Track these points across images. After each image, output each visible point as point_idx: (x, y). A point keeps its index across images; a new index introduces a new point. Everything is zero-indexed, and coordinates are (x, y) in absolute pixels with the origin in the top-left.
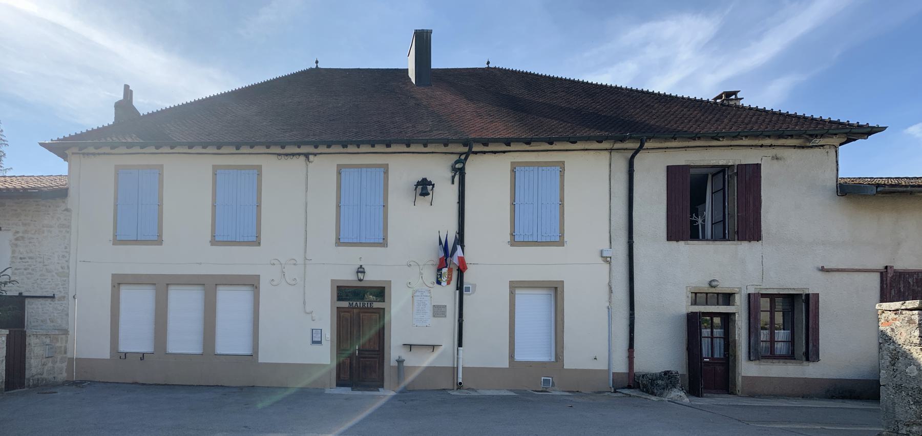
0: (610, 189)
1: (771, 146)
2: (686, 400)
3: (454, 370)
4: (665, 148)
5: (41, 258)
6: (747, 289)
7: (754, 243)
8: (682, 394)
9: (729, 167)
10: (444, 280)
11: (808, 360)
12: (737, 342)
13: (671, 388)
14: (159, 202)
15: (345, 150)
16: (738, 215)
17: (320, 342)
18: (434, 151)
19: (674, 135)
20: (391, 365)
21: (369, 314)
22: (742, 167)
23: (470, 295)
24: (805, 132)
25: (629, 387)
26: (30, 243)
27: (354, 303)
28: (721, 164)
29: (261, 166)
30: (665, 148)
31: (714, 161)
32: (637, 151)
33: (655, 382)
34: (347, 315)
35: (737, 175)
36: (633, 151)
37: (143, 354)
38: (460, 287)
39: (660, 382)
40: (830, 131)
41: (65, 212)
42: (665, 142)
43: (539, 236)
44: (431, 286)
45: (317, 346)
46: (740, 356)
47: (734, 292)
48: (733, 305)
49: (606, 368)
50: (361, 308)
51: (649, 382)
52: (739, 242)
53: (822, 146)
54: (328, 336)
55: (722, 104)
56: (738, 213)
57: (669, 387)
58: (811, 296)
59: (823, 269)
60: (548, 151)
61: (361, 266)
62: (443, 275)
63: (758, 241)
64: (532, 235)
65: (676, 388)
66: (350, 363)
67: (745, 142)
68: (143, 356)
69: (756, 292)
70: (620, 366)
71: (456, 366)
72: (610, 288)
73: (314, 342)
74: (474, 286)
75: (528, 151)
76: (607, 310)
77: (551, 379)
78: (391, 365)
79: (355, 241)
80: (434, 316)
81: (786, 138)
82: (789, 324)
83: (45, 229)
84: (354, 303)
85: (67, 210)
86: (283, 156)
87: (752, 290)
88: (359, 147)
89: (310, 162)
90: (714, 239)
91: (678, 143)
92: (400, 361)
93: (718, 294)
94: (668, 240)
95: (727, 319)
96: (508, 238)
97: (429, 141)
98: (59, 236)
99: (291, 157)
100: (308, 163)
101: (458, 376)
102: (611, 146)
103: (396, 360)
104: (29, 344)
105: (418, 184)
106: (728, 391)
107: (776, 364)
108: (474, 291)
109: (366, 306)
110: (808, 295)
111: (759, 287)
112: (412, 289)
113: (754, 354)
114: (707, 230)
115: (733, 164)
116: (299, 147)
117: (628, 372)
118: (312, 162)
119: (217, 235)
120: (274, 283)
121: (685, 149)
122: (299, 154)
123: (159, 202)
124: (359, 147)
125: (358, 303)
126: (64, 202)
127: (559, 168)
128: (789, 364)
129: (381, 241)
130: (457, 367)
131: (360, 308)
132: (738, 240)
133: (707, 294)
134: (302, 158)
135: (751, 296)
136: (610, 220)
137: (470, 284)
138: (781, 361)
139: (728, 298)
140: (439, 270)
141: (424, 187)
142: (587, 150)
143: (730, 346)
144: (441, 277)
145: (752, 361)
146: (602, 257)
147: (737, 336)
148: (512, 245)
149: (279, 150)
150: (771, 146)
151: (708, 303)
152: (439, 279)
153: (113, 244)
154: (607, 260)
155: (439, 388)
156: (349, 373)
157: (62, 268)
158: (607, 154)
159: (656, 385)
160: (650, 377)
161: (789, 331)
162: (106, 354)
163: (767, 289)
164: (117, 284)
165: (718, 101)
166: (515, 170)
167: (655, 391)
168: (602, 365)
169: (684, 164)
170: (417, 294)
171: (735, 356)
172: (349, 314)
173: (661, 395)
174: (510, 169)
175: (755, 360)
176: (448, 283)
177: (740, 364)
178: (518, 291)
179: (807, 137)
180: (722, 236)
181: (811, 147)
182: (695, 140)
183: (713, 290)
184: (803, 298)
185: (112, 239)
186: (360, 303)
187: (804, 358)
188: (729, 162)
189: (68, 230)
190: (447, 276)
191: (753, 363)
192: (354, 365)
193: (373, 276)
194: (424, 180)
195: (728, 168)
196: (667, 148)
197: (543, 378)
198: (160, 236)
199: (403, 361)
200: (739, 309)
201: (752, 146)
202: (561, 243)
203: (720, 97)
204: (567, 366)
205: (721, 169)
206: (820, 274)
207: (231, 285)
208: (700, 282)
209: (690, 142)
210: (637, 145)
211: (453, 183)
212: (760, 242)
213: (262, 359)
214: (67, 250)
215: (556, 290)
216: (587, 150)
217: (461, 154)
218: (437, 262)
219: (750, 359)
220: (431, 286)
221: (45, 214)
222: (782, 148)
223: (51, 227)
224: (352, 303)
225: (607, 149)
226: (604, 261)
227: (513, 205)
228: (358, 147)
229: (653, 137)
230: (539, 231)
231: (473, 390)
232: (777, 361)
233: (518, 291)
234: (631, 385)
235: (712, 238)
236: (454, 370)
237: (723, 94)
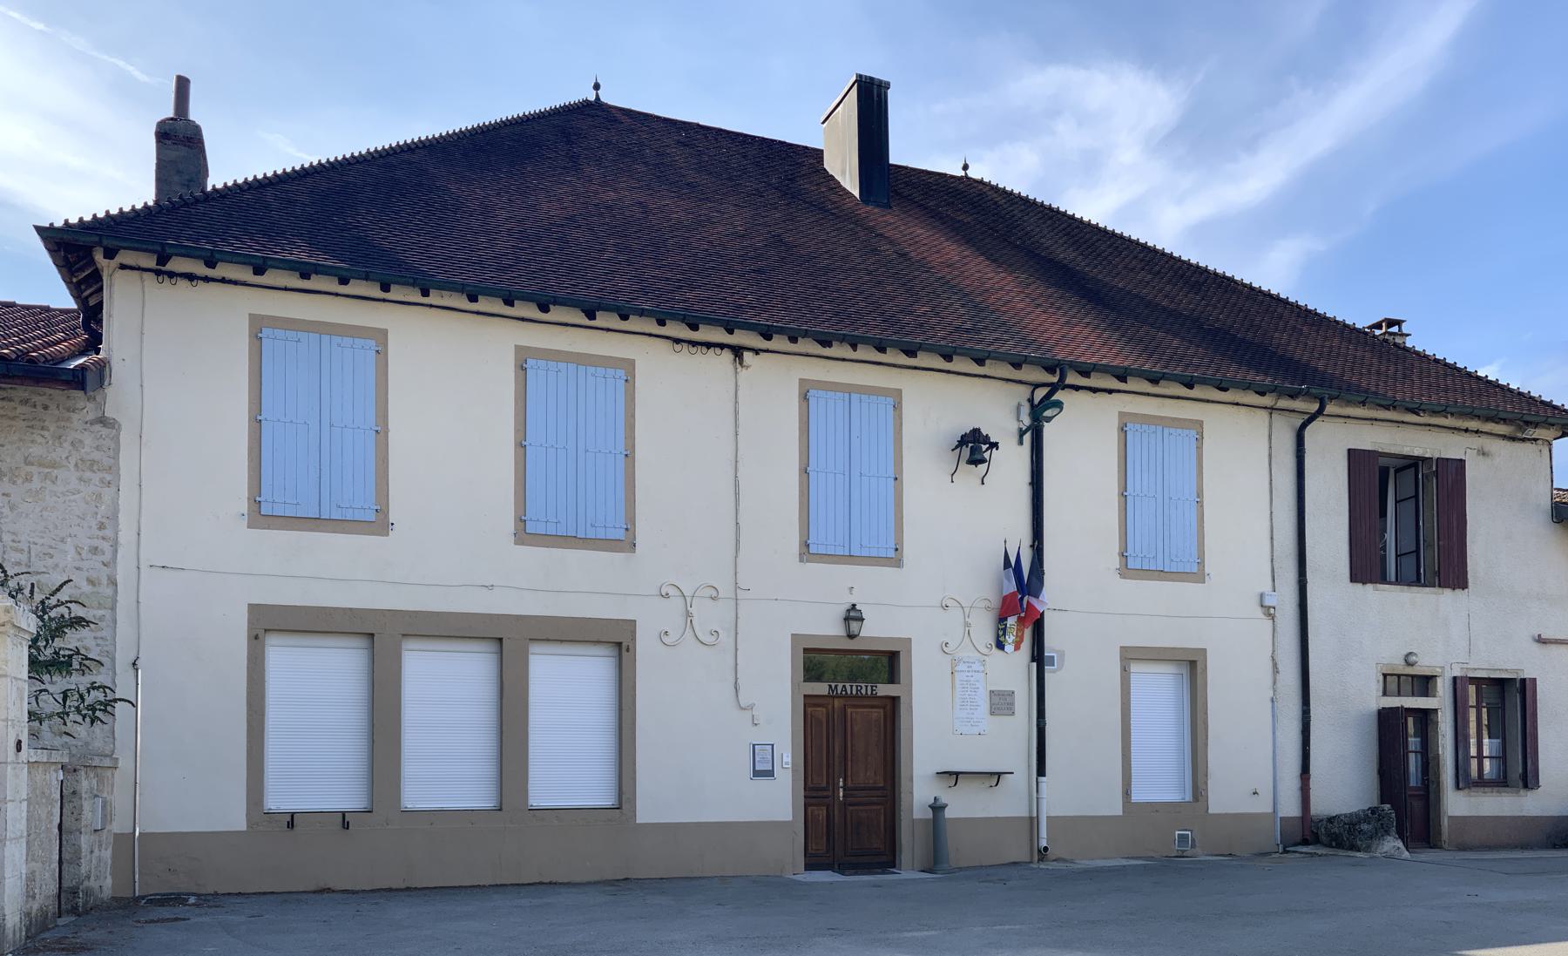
0: (1271, 480)
1: (1477, 432)
2: (1406, 854)
3: (1032, 822)
7: (1458, 591)
8: (1400, 844)
9: (1424, 459)
11: (1526, 786)
12: (1441, 758)
13: (1382, 836)
14: (626, 450)
15: (827, 352)
17: (770, 774)
19: (1365, 397)
20: (914, 817)
21: (865, 710)
22: (1443, 462)
23: (1054, 672)
25: (1305, 842)
31: (1408, 449)
32: (1313, 418)
34: (821, 712)
36: (1306, 417)
37: (293, 815)
38: (1039, 656)
39: (1365, 827)
40: (1550, 420)
41: (98, 427)
43: (1167, 561)
44: (985, 651)
45: (763, 783)
47: (1435, 674)
48: (1434, 696)
49: (1270, 810)
50: (855, 697)
52: (1440, 590)
53: (1536, 440)
54: (788, 758)
55: (1381, 338)
56: (1438, 541)
58: (1528, 682)
59: (1541, 640)
60: (1178, 398)
61: (854, 605)
64: (1155, 557)
65: (1389, 835)
68: (344, 820)
69: (1463, 674)
70: (1290, 808)
71: (1035, 815)
72: (1275, 665)
73: (757, 773)
74: (1062, 654)
75: (1148, 394)
77: (1189, 833)
78: (914, 817)
80: (992, 713)
81: (1496, 423)
82: (1497, 728)
83: (33, 469)
84: (840, 686)
85: (103, 421)
86: (685, 345)
87: (1457, 673)
88: (855, 350)
89: (742, 367)
90: (1399, 581)
92: (937, 808)
93: (1413, 676)
94: (1351, 581)
96: (1116, 561)
100: (739, 369)
101: (1040, 836)
102: (1274, 403)
103: (930, 806)
104: (74, 793)
105: (963, 441)
106: (1429, 843)
107: (1488, 794)
108: (1060, 668)
109: (863, 691)
110: (1523, 681)
111: (1465, 666)
112: (950, 657)
113: (1464, 781)
116: (731, 332)
119: (531, 520)
120: (665, 639)
122: (722, 346)
123: (626, 450)
124: (855, 350)
125: (848, 685)
126: (91, 399)
127: (1195, 432)
128: (1503, 794)
129: (892, 554)
130: (1038, 816)
132: (1440, 586)
133: (1399, 676)
134: (727, 356)
135: (1458, 681)
136: (1272, 538)
138: (1496, 789)
140: (1002, 619)
141: (974, 446)
142: (1237, 404)
143: (1430, 765)
144: (1004, 634)
145: (1461, 789)
149: (683, 332)
150: (1477, 432)
152: (1002, 639)
154: (1269, 612)
155: (1006, 862)
156: (825, 838)
157: (91, 582)
158: (1264, 414)
159: (1359, 832)
160: (1346, 820)
161: (1498, 741)
162: (236, 820)
163: (1475, 669)
165: (1378, 332)
166: (1125, 429)
167: (1359, 843)
168: (1262, 806)
169: (1370, 449)
170: (961, 667)
171: (1438, 783)
172: (824, 710)
173: (1368, 849)
175: (1465, 788)
176: (1017, 648)
177: (1445, 796)
178: (1135, 668)
179: (1522, 424)
180: (1415, 579)
181: (1524, 440)
183: (1410, 671)
184: (1518, 685)
185: (246, 512)
186: (851, 686)
187: (1521, 784)
189: (108, 478)
191: (1461, 793)
193: (877, 629)
195: (1423, 461)
196: (1349, 417)
197: (1177, 832)
198: (382, 511)
199: (943, 807)
200: (1440, 701)
201: (1455, 429)
203: (1378, 326)
204: (1213, 809)
205: (1412, 461)
206: (1536, 646)
207: (562, 641)
208: (1393, 658)
210: (1315, 407)
211: (1021, 443)
212: (1466, 590)
213: (646, 812)
215: (1192, 666)
216: (1237, 404)
217: (1037, 386)
218: (996, 602)
219: (1458, 787)
220: (985, 651)
221: (32, 427)
222: (1489, 437)
223: (54, 465)
224: (836, 686)
225: (1266, 408)
227: (1123, 495)
230: (1166, 554)
231: (1065, 860)
232: (1490, 789)
233: (1135, 668)
234: (1308, 837)
236: (1032, 822)
237: (1383, 321)
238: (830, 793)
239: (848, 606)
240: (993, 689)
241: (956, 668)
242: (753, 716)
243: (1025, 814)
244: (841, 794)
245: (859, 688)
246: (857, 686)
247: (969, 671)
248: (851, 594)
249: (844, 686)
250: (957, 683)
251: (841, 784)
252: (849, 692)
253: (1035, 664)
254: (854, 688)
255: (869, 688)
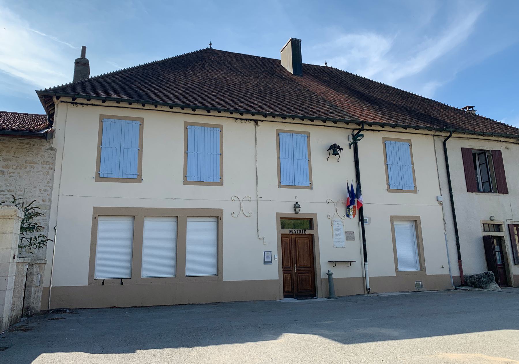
0: (436, 159)
2: (500, 289)
3: (364, 279)
4: (459, 137)
5: (22, 191)
6: (507, 222)
7: (505, 194)
9: (487, 151)
10: (351, 214)
12: (507, 253)
16: (496, 179)
17: (270, 262)
18: (338, 126)
24: (501, 135)
25: (462, 285)
26: (10, 177)
27: (293, 230)
28: (484, 149)
29: (223, 125)
30: (459, 137)
31: (481, 147)
32: (448, 138)
33: (481, 279)
35: (492, 156)
36: (446, 138)
37: (104, 279)
38: (361, 219)
39: (484, 279)
42: (459, 134)
43: (404, 186)
44: (343, 218)
45: (268, 265)
46: (510, 262)
51: (476, 280)
52: (499, 194)
54: (276, 256)
56: (496, 177)
57: (489, 282)
60: (402, 132)
61: (297, 203)
62: (350, 210)
63: (507, 194)
64: (399, 185)
65: (493, 282)
66: (291, 277)
67: (494, 138)
68: (121, 281)
72: (444, 221)
73: (266, 262)
74: (370, 219)
75: (392, 131)
76: (444, 235)
77: (420, 282)
79: (291, 184)
80: (347, 240)
81: (510, 138)
85: (51, 149)
90: (484, 191)
91: (495, 138)
93: (494, 224)
95: (500, 239)
96: (386, 187)
97: (397, 125)
98: (42, 171)
99: (245, 121)
105: (331, 148)
106: (507, 285)
108: (370, 223)
109: (301, 232)
112: (331, 220)
114: (480, 186)
115: (489, 150)
116: (253, 115)
117: (460, 275)
118: (259, 126)
120: (233, 215)
121: (488, 140)
122: (251, 120)
123: (220, 153)
125: (296, 230)
127: (139, 122)
130: (366, 277)
131: (296, 234)
134: (253, 123)
135: (510, 226)
137: (368, 218)
139: (498, 227)
140: (348, 207)
141: (335, 150)
142: (422, 134)
144: (349, 212)
145: (516, 265)
146: (438, 201)
147: (507, 251)
148: (96, 181)
149: (239, 116)
151: (490, 231)
152: (348, 213)
153: (96, 181)
154: (440, 203)
157: (43, 201)
158: (432, 137)
160: (477, 277)
164: (350, 217)
168: (446, 272)
174: (382, 142)
176: (354, 217)
178: (395, 223)
182: (473, 135)
186: (297, 231)
188: (488, 148)
189: (51, 166)
190: (353, 211)
192: (294, 279)
193: (305, 211)
194: (335, 145)
197: (416, 282)
200: (504, 233)
202: (139, 179)
209: (470, 136)
210: (448, 134)
211: (350, 148)
213: (227, 277)
214: (49, 185)
215: (415, 222)
216: (422, 134)
217: (354, 130)
218: (345, 201)
220: (343, 218)
221: (29, 151)
224: (292, 231)
226: (439, 204)
228: (294, 119)
229: (455, 131)
230: (403, 183)
231: (377, 293)
233: (395, 223)
235: (483, 191)
238: (291, 269)
239: (295, 203)
240: (346, 231)
241: (333, 224)
242: (264, 241)
243: (361, 276)
244: (295, 269)
245: (300, 231)
246: (299, 230)
247: (337, 225)
248: (296, 199)
249: (295, 230)
250: (334, 229)
251: (295, 266)
252: (296, 233)
253: (361, 222)
254: (298, 231)
255: (303, 231)
